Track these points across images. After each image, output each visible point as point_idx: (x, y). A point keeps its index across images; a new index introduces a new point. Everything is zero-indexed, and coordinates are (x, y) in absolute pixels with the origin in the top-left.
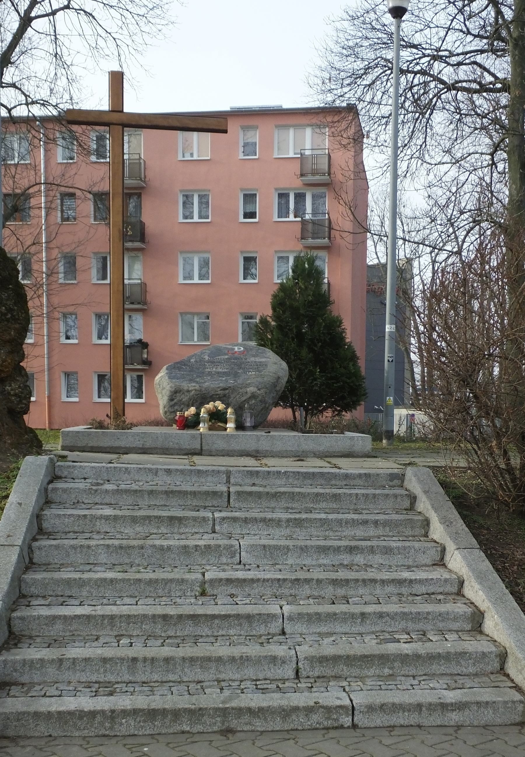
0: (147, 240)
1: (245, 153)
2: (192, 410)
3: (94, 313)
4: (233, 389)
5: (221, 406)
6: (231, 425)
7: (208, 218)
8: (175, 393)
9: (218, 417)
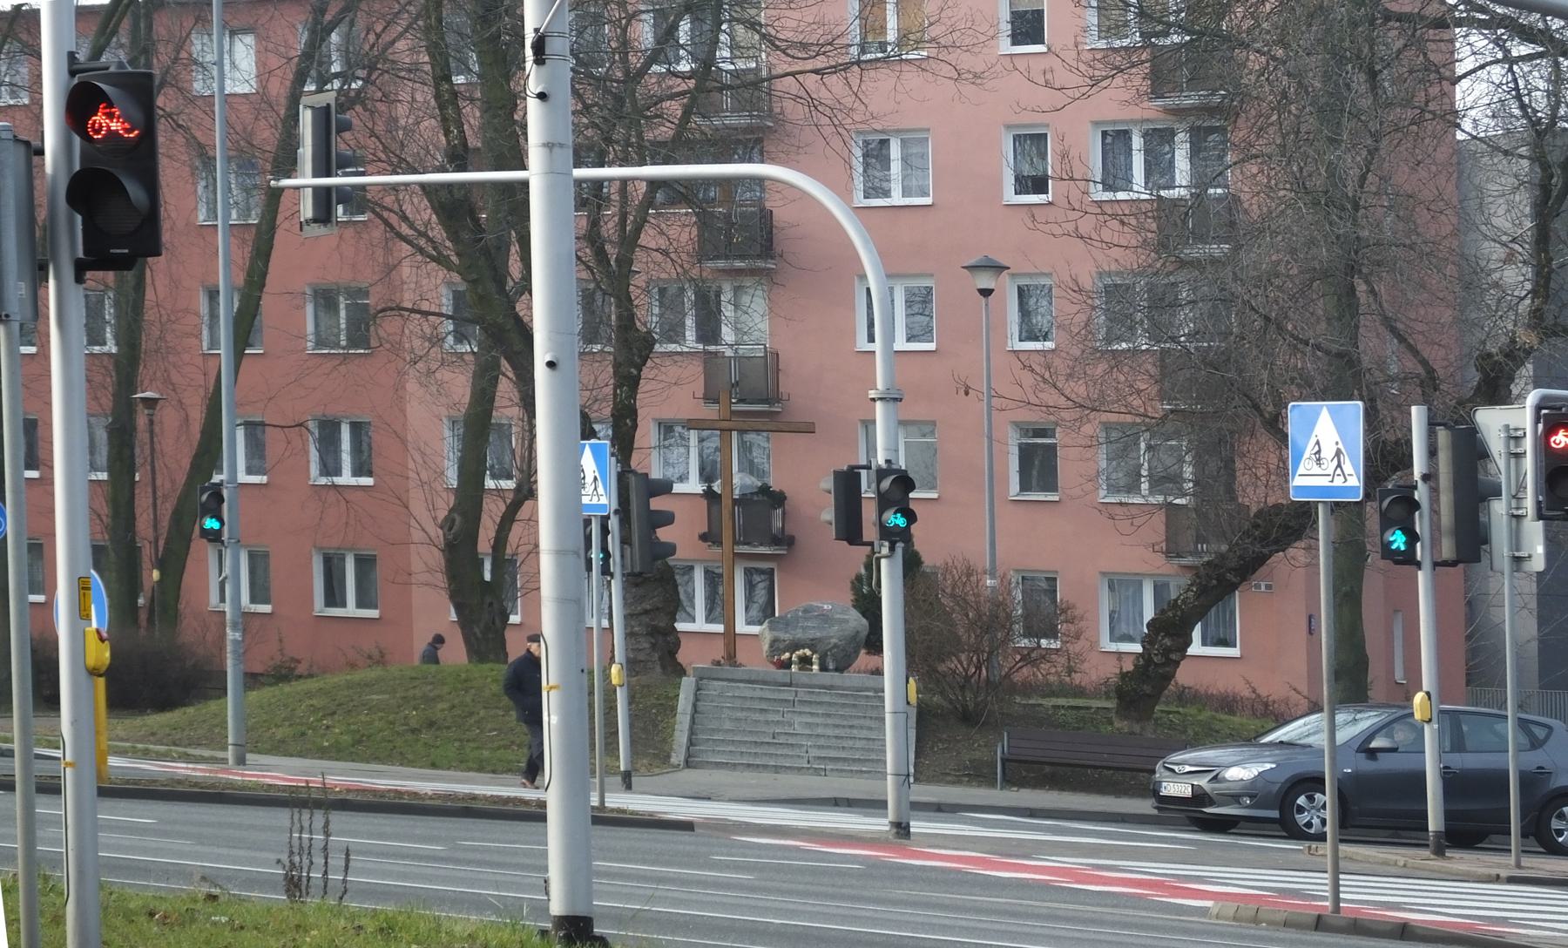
0: (778, 248)
1: (1017, 39)
2: (787, 655)
3: (655, 420)
4: (820, 640)
5: (808, 652)
6: (815, 667)
7: (925, 194)
8: (774, 642)
9: (805, 662)
